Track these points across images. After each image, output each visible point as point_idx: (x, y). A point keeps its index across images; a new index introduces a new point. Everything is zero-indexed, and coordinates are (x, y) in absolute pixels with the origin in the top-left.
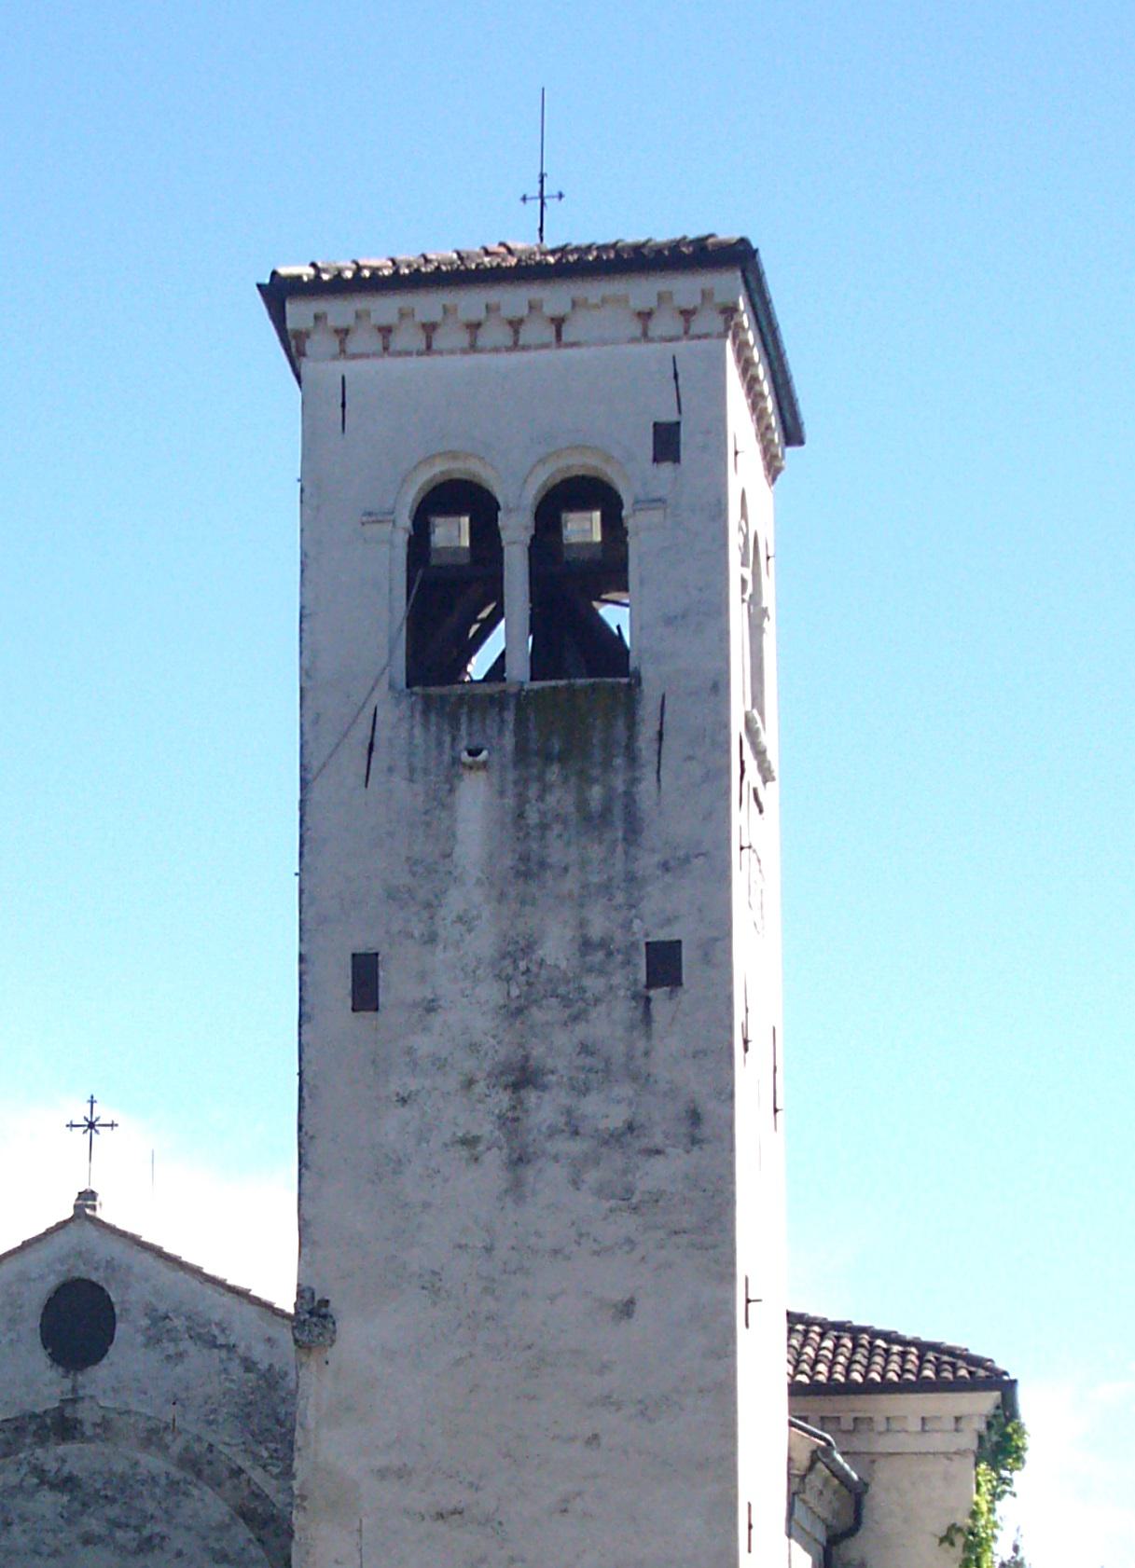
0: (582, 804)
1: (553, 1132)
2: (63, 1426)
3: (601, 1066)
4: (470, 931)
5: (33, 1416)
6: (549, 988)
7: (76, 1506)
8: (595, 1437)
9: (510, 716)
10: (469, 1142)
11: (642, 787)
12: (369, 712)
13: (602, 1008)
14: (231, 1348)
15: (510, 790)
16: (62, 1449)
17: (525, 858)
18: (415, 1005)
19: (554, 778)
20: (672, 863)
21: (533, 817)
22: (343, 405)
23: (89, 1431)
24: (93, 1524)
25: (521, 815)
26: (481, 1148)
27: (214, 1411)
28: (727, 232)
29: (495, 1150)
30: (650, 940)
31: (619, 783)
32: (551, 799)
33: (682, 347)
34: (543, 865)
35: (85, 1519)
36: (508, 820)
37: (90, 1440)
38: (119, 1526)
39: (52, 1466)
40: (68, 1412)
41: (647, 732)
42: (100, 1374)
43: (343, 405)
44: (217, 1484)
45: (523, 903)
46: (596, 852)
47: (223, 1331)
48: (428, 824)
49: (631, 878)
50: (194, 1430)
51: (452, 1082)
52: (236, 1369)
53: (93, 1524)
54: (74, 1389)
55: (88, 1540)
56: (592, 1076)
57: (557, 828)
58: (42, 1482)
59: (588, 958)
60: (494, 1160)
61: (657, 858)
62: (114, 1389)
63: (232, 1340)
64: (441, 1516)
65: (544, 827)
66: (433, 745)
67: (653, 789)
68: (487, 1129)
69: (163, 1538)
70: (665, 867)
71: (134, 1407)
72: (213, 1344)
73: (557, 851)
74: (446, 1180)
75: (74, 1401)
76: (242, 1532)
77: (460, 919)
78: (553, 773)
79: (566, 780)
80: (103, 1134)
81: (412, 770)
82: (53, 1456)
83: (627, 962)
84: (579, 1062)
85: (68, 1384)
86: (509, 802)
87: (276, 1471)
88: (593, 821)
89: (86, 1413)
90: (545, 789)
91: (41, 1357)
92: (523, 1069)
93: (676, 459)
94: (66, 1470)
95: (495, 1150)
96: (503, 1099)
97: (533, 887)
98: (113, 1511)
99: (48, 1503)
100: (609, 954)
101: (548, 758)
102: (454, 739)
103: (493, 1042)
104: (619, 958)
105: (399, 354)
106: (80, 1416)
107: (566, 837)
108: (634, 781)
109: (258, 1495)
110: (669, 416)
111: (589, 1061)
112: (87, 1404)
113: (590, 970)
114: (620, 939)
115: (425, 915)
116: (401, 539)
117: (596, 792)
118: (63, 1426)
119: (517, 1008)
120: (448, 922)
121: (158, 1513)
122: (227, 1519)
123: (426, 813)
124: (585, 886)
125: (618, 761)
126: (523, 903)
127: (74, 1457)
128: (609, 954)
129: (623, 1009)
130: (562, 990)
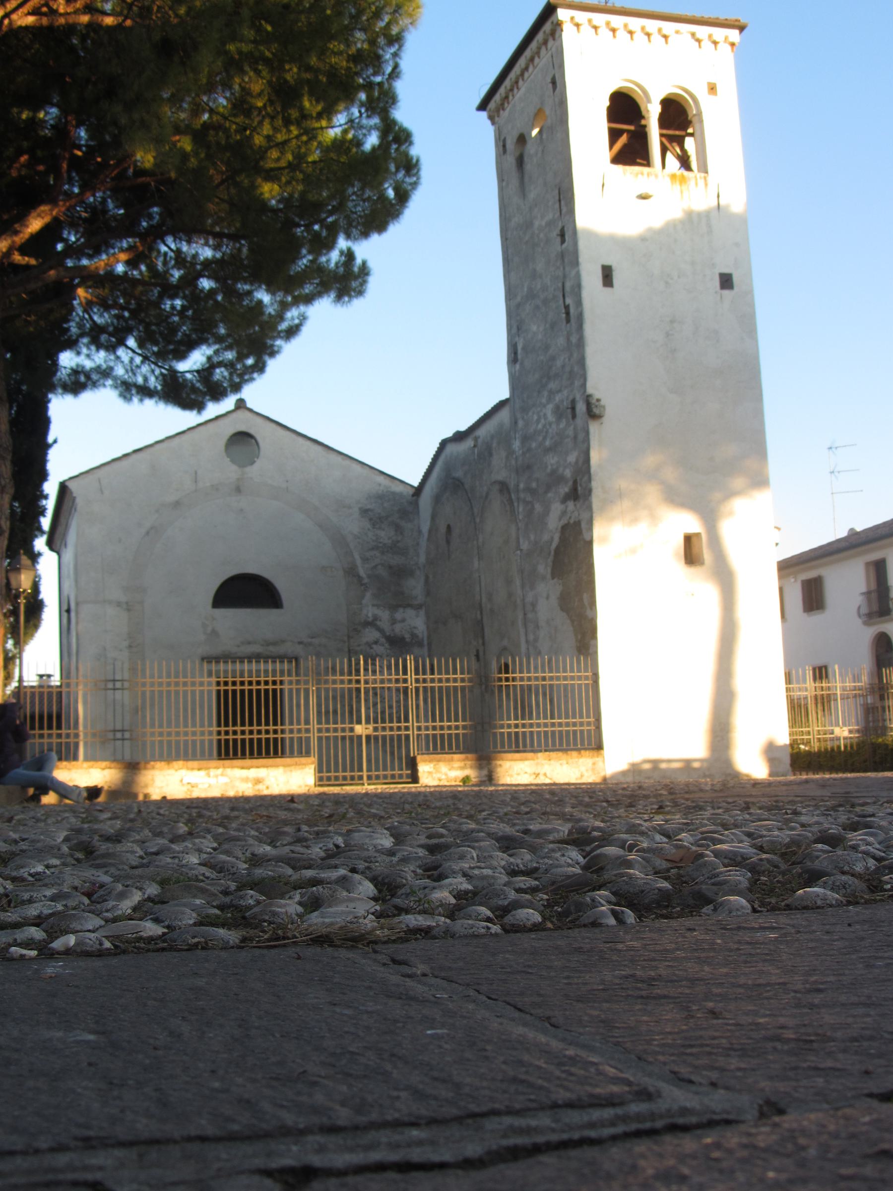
42: (253, 471)
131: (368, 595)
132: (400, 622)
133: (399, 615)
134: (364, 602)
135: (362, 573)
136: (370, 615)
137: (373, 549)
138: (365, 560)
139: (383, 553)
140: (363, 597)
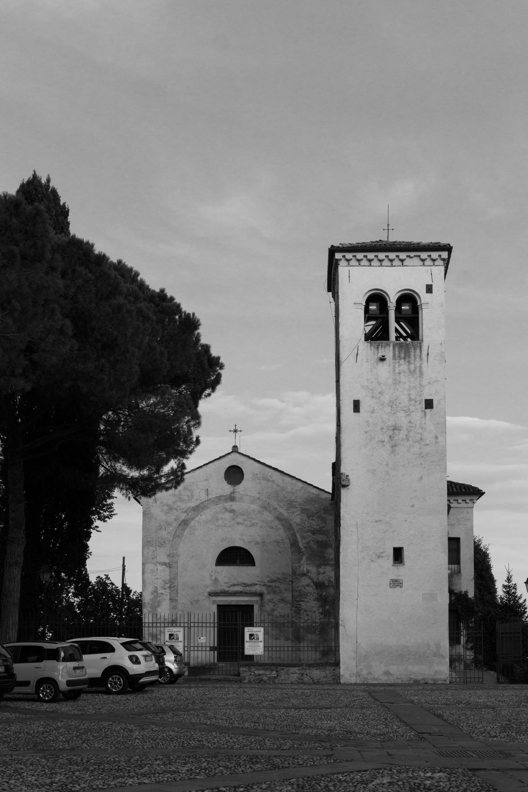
0: (409, 369)
1: (403, 440)
2: (231, 498)
3: (414, 426)
4: (382, 396)
5: (223, 496)
6: (401, 408)
7: (235, 516)
8: (413, 505)
9: (391, 348)
10: (383, 442)
11: (423, 365)
12: (357, 346)
13: (414, 413)
14: (274, 481)
15: (392, 365)
16: (231, 503)
17: (395, 380)
18: (368, 412)
19: (402, 363)
20: (431, 382)
21: (397, 371)
22: (349, 277)
23: (237, 499)
24: (240, 520)
25: (394, 370)
26: (385, 443)
27: (269, 495)
28: (444, 241)
29: (388, 444)
30: (426, 399)
31: (418, 365)
32: (402, 368)
33: (433, 268)
34: (400, 382)
35: (237, 519)
36: (391, 371)
37: (238, 501)
38: (246, 520)
39: (228, 507)
40: (232, 495)
41: (424, 353)
42: (240, 488)
43: (349, 277)
44: (270, 512)
45: (395, 390)
46: (412, 380)
47: (271, 478)
48: (371, 372)
49: (421, 385)
50: (265, 499)
51: (378, 429)
52: (274, 486)
53: (240, 520)
54: (234, 490)
55: (238, 523)
56: (412, 428)
57: (403, 374)
58: (226, 511)
59: (411, 402)
60: (388, 446)
61: (427, 381)
62: (244, 490)
63: (274, 480)
64: (376, 522)
65: (400, 373)
66: (373, 354)
67: (426, 366)
68: (386, 439)
69: (257, 523)
70: (429, 383)
71: (249, 494)
72: (269, 480)
73: (403, 379)
74: (377, 450)
75: (234, 493)
76: (277, 522)
77: (380, 393)
78: (402, 361)
79: (405, 363)
80: (238, 433)
81: (367, 360)
82: (228, 505)
83: (420, 403)
84: (408, 425)
85: (232, 489)
86: (391, 368)
87: (284, 508)
88: (412, 373)
89: (236, 495)
90: (400, 365)
91: (225, 482)
92: (395, 426)
93: (432, 292)
94: (232, 508)
95: (388, 444)
96: (391, 433)
97: (397, 386)
98: (244, 517)
99: (227, 515)
100: (416, 401)
101: (400, 358)
102: (378, 353)
103: (388, 420)
104: (418, 402)
105: (362, 266)
106: (235, 496)
107: (405, 375)
108: (421, 364)
109: (281, 514)
110: (430, 283)
111: (411, 425)
112: (237, 493)
113: (411, 405)
114: (418, 399)
115: (371, 392)
116: (363, 307)
117: (412, 367)
118: (231, 498)
119: (208, 394)
120: (377, 393)
121: (255, 518)
122: (273, 519)
123: (371, 369)
124: (410, 386)
125: (418, 359)
126: (395, 390)
127: (235, 505)
128: (416, 401)
129: (420, 414)
130: (404, 409)
131: (304, 558)
132: (322, 574)
133: (321, 570)
134: (302, 562)
135: (301, 545)
136: (305, 570)
137: (308, 532)
138: (303, 538)
139: (314, 534)
140: (300, 559)
